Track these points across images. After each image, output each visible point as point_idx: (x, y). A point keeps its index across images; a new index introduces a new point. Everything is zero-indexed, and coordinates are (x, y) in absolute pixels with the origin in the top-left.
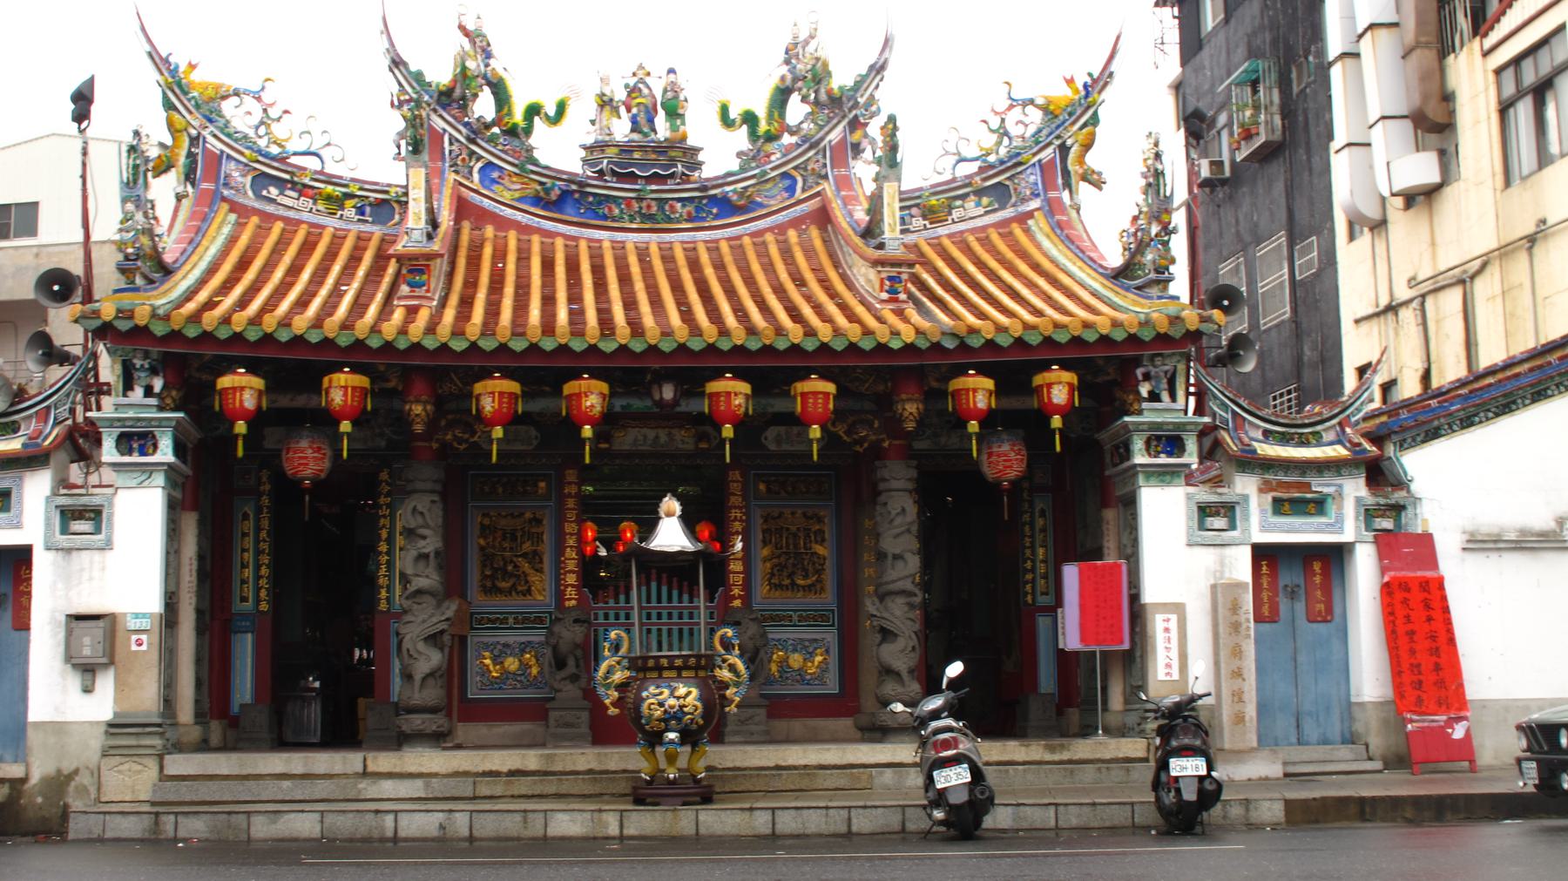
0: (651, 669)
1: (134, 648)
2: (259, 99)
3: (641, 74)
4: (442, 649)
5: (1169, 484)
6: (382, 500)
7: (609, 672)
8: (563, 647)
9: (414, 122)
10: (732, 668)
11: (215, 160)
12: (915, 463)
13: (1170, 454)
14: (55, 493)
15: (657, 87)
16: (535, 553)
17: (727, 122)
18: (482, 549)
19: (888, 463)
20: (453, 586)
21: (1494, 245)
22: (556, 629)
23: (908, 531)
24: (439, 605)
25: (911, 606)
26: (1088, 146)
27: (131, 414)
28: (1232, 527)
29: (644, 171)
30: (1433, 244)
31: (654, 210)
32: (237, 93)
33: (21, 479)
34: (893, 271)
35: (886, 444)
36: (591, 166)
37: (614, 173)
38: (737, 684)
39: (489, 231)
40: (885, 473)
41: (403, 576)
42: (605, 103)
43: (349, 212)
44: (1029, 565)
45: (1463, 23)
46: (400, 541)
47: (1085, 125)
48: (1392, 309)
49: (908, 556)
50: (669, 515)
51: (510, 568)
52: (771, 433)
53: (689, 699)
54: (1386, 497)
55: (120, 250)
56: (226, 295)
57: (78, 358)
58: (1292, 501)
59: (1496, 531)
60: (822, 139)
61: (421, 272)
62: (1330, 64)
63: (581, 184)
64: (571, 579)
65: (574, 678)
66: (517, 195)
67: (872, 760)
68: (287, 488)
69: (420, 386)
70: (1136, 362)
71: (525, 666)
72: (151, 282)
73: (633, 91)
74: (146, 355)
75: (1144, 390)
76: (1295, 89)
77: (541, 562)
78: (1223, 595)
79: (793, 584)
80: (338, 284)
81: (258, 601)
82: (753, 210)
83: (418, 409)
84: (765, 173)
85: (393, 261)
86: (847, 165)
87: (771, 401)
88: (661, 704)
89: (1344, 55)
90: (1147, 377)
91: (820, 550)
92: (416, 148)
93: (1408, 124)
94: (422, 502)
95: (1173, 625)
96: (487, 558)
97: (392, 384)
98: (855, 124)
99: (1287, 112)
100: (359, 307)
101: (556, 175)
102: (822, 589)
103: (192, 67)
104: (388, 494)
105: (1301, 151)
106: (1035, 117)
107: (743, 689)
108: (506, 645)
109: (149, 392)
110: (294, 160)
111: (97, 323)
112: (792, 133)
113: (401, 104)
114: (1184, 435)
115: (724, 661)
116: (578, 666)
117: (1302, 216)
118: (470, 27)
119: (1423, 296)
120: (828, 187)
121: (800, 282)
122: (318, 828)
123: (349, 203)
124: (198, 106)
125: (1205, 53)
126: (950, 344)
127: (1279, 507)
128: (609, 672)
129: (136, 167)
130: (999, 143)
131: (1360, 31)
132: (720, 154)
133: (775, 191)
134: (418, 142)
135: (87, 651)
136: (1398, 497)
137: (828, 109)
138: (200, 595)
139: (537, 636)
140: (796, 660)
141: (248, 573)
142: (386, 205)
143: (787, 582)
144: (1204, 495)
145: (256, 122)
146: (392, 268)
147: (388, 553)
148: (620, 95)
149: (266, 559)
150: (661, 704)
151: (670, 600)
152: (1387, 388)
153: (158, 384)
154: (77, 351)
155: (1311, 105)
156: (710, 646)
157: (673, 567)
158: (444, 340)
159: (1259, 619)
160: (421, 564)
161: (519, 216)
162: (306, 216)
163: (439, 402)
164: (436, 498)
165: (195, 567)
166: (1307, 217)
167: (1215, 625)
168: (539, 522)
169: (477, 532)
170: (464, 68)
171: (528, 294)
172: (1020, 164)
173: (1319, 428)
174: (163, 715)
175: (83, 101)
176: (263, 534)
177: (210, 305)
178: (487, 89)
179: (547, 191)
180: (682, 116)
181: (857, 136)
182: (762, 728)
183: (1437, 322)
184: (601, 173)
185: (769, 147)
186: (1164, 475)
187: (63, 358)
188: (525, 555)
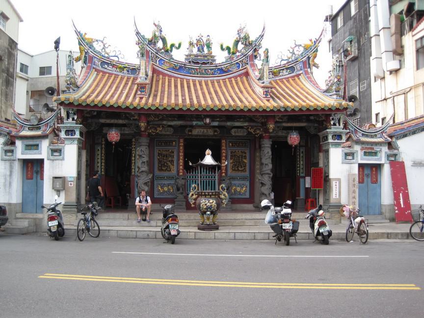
0: (203, 195)
1: (70, 185)
2: (103, 42)
3: (200, 37)
4: (148, 186)
5: (338, 147)
6: (133, 146)
7: (193, 195)
8: (179, 186)
9: (142, 49)
10: (224, 195)
11: (91, 58)
12: (271, 140)
13: (338, 140)
14: (50, 145)
15: (205, 40)
16: (172, 160)
17: (222, 49)
18: (158, 159)
19: (265, 140)
20: (151, 171)
21: (413, 85)
22: (177, 181)
23: (269, 158)
24: (148, 175)
25: (269, 177)
26: (315, 57)
27: (69, 125)
28: (353, 159)
29: (200, 63)
30: (397, 84)
31: (203, 72)
32: (97, 41)
33: (41, 141)
34: (267, 90)
35: (264, 135)
36: (187, 60)
37: (193, 62)
38: (225, 199)
39: (161, 76)
40: (264, 142)
41: (138, 167)
42: (191, 44)
43: (125, 71)
44: (298, 166)
45: (407, 27)
46: (137, 157)
47: (314, 52)
48: (385, 99)
49: (269, 164)
50: (208, 154)
51: (166, 164)
52: (233, 130)
53: (213, 203)
54: (393, 152)
55: (66, 82)
56: (93, 94)
57: (56, 110)
58: (369, 152)
59: (420, 161)
60: (247, 54)
61: (144, 88)
62: (371, 37)
63: (185, 65)
64: (181, 167)
65: (182, 193)
66: (168, 67)
67: (259, 218)
68: (108, 144)
69: (143, 118)
70: (330, 115)
71: (169, 190)
72: (74, 90)
73: (198, 41)
74: (73, 110)
75: (332, 123)
76: (361, 44)
77: (174, 163)
78: (350, 175)
79: (238, 170)
80: (122, 90)
81: (101, 172)
82: (229, 72)
83: (142, 124)
84: (232, 62)
85: (136, 85)
86: (253, 61)
87: (234, 123)
88: (206, 205)
89: (376, 35)
90: (333, 119)
91: (245, 160)
92: (143, 55)
93: (391, 53)
94: (143, 148)
95: (337, 184)
96: (160, 162)
97: (136, 118)
98: (255, 50)
99: (359, 49)
100: (127, 96)
101: (178, 62)
102: (246, 171)
103: (86, 34)
104: (135, 145)
105: (363, 59)
106: (302, 49)
107: (227, 201)
108: (164, 184)
109: (73, 119)
110: (111, 58)
111: (60, 102)
112: (239, 52)
113: (139, 44)
114: (342, 135)
115: (222, 193)
116: (183, 190)
117: (362, 76)
118: (157, 24)
119: (394, 97)
120: (248, 66)
121: (241, 92)
122: (116, 234)
123: (125, 69)
124: (87, 44)
125: (338, 33)
126: (282, 110)
127: (366, 154)
128: (193, 195)
129: (70, 61)
130: (292, 56)
131: (380, 29)
132: (220, 57)
133: (235, 67)
134: (143, 54)
135: (58, 186)
136: (395, 152)
137: (248, 48)
138: (86, 171)
139: (172, 182)
140: (238, 189)
141: (99, 165)
142: (134, 70)
143: (237, 169)
144: (347, 150)
145: (102, 48)
146: (136, 87)
147: (134, 160)
148: (195, 42)
149: (103, 161)
150: (206, 205)
151: (209, 173)
152: (383, 119)
153: (76, 117)
154: (55, 108)
155: (366, 47)
156: (219, 189)
157: (211, 168)
158: (149, 107)
159: (359, 182)
160: (143, 164)
161: (168, 73)
162: (114, 72)
163: (148, 122)
164: (147, 147)
165: (85, 164)
166: (364, 76)
167: (349, 187)
168: (173, 152)
169: (157, 155)
170: (155, 35)
171: (171, 94)
172: (297, 61)
173: (376, 133)
174: (77, 203)
175: (57, 43)
176: (103, 155)
177: (89, 96)
178: (160, 40)
179: (176, 66)
180: (211, 48)
181: (256, 54)
182: (229, 207)
183: (397, 103)
184: (190, 62)
185: (233, 56)
186: (337, 145)
187: (52, 110)
188: (169, 161)
